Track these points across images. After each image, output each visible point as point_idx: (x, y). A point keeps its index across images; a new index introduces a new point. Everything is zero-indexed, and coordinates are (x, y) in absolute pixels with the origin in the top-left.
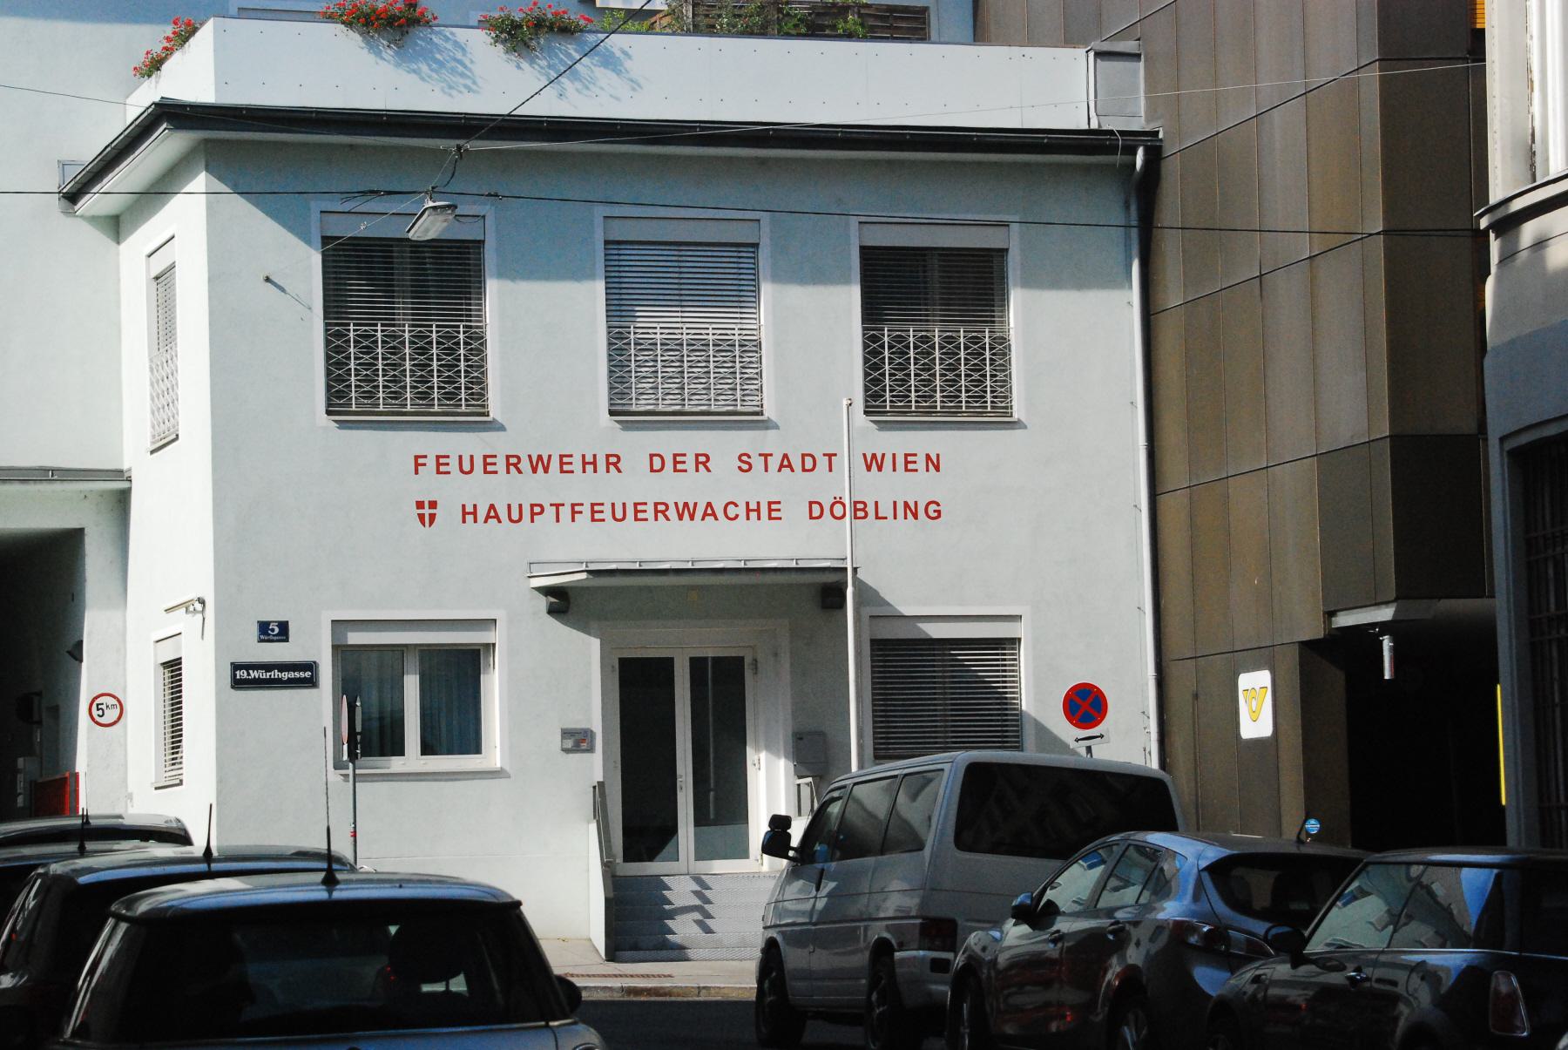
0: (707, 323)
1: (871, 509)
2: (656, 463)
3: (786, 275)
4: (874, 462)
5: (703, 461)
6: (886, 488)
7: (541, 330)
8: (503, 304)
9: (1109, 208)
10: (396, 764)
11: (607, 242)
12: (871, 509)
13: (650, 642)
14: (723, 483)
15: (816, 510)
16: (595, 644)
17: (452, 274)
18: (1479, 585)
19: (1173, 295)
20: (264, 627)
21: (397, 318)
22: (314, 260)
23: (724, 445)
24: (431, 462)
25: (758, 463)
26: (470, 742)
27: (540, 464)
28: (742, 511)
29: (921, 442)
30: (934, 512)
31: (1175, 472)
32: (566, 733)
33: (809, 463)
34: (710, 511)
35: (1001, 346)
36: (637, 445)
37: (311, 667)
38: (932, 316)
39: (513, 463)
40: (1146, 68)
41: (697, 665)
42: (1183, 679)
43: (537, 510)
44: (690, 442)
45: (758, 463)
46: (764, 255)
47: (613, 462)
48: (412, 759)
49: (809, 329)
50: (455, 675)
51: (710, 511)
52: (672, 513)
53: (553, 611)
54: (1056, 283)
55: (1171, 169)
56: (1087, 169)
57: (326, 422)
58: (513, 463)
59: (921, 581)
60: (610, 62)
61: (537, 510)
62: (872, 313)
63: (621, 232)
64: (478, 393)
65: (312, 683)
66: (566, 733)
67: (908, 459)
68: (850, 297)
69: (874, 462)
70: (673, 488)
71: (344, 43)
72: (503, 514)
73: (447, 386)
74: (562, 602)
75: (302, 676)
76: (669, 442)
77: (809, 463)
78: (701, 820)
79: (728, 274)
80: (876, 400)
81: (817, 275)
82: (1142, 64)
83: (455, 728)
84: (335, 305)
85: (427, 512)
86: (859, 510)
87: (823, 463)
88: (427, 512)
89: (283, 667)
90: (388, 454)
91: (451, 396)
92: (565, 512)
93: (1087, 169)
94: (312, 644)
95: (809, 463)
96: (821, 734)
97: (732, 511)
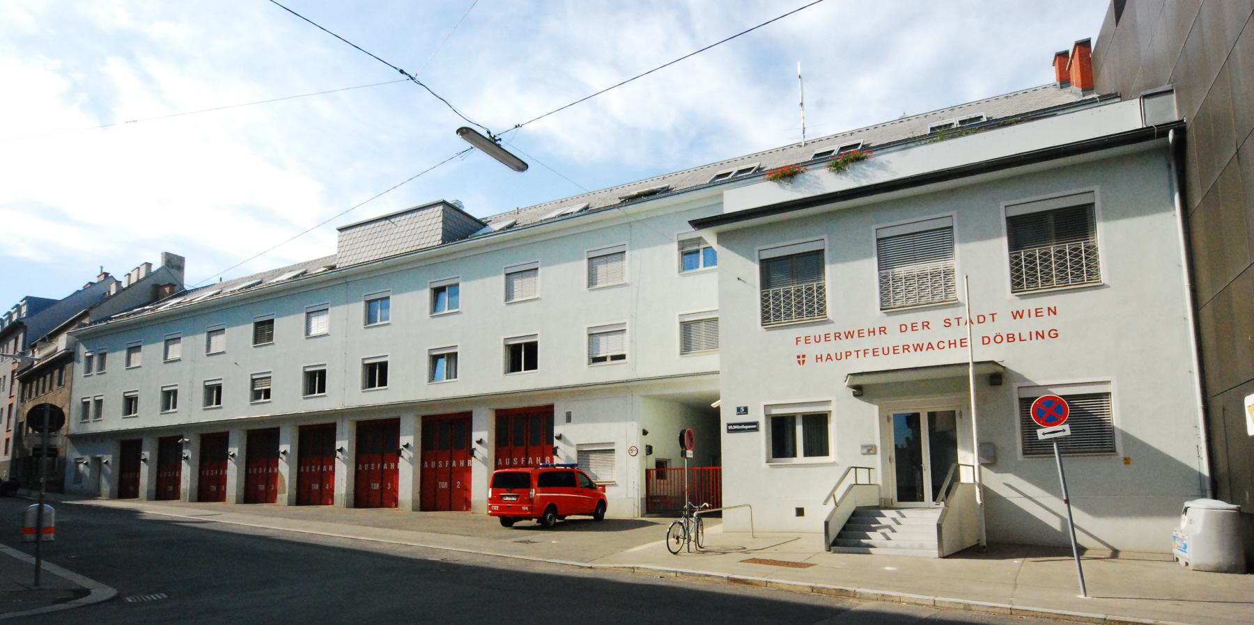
1: (1017, 337)
2: (903, 329)
3: (965, 240)
4: (1018, 315)
5: (926, 325)
6: (1026, 326)
7: (850, 281)
10: (794, 460)
11: (878, 240)
12: (1017, 337)
13: (909, 406)
14: (937, 333)
15: (986, 340)
16: (876, 408)
17: (812, 264)
19: (1196, 201)
20: (739, 409)
21: (791, 283)
23: (936, 317)
24: (803, 340)
25: (954, 322)
26: (823, 451)
27: (849, 335)
28: (947, 344)
29: (1045, 302)
30: (1054, 334)
31: (1206, 295)
32: (863, 447)
33: (981, 319)
34: (930, 346)
35: (1091, 251)
36: (893, 322)
37: (756, 423)
38: (1052, 241)
39: (838, 336)
41: (932, 416)
43: (848, 354)
45: (954, 322)
46: (955, 229)
47: (883, 330)
48: (800, 458)
49: (982, 261)
50: (817, 425)
51: (930, 346)
52: (911, 349)
53: (855, 395)
54: (1125, 215)
55: (1192, 137)
56: (1141, 154)
57: (761, 329)
58: (838, 336)
59: (1045, 368)
61: (848, 354)
62: (1014, 245)
64: (822, 311)
65: (756, 429)
66: (863, 447)
67: (807, 339)
68: (1004, 242)
69: (1018, 315)
70: (911, 338)
71: (773, 186)
73: (813, 308)
74: (859, 391)
75: (753, 427)
76: (908, 319)
77: (981, 319)
79: (938, 242)
80: (1017, 284)
81: (984, 235)
82: (1174, 95)
85: (801, 359)
86: (1011, 338)
87: (989, 318)
88: (801, 359)
89: (746, 424)
90: (786, 338)
91: (800, 314)
92: (861, 353)
93: (1141, 154)
94: (758, 415)
95: (981, 319)
97: (941, 345)
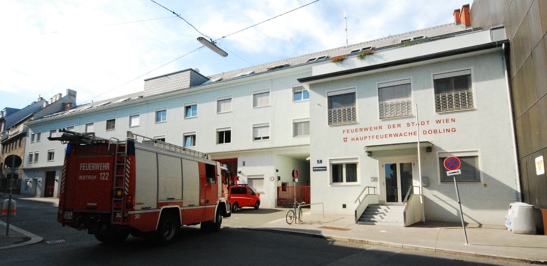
0: (405, 100)
1: (438, 131)
2: (389, 127)
4: (438, 122)
5: (408, 125)
6: (441, 127)
7: (367, 106)
8: (359, 103)
9: (499, 63)
10: (342, 184)
11: (379, 88)
12: (438, 131)
14: (404, 129)
18: (117, 165)
19: (514, 73)
20: (318, 161)
21: (341, 106)
22: (326, 100)
23: (403, 122)
27: (366, 129)
28: (408, 134)
29: (450, 116)
30: (454, 130)
31: (519, 114)
32: (372, 178)
33: (423, 123)
35: (470, 95)
36: (385, 124)
37: (314, 170)
38: (453, 89)
39: (361, 130)
40: (506, 30)
42: (523, 166)
43: (366, 138)
44: (396, 122)
45: (411, 125)
47: (381, 127)
48: (345, 182)
49: (423, 98)
50: (352, 168)
54: (484, 79)
55: (512, 47)
58: (361, 130)
59: (450, 145)
60: (377, 56)
61: (366, 138)
62: (437, 92)
63: (381, 86)
64: (354, 119)
65: (326, 170)
69: (438, 122)
70: (393, 131)
72: (359, 139)
74: (370, 154)
75: (324, 169)
76: (391, 123)
77: (423, 123)
78: (456, 182)
79: (404, 90)
81: (424, 87)
83: (352, 177)
84: (330, 106)
85: (345, 140)
86: (435, 132)
87: (426, 123)
88: (345, 140)
90: (339, 130)
91: (345, 120)
92: (371, 137)
93: (491, 53)
95: (423, 123)
96: (428, 178)
97: (406, 134)
